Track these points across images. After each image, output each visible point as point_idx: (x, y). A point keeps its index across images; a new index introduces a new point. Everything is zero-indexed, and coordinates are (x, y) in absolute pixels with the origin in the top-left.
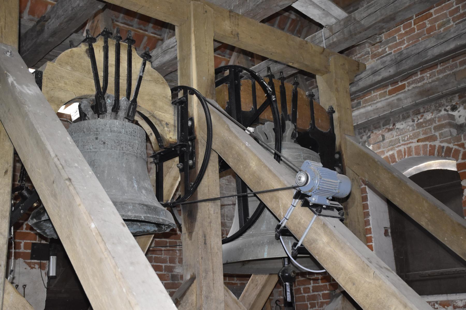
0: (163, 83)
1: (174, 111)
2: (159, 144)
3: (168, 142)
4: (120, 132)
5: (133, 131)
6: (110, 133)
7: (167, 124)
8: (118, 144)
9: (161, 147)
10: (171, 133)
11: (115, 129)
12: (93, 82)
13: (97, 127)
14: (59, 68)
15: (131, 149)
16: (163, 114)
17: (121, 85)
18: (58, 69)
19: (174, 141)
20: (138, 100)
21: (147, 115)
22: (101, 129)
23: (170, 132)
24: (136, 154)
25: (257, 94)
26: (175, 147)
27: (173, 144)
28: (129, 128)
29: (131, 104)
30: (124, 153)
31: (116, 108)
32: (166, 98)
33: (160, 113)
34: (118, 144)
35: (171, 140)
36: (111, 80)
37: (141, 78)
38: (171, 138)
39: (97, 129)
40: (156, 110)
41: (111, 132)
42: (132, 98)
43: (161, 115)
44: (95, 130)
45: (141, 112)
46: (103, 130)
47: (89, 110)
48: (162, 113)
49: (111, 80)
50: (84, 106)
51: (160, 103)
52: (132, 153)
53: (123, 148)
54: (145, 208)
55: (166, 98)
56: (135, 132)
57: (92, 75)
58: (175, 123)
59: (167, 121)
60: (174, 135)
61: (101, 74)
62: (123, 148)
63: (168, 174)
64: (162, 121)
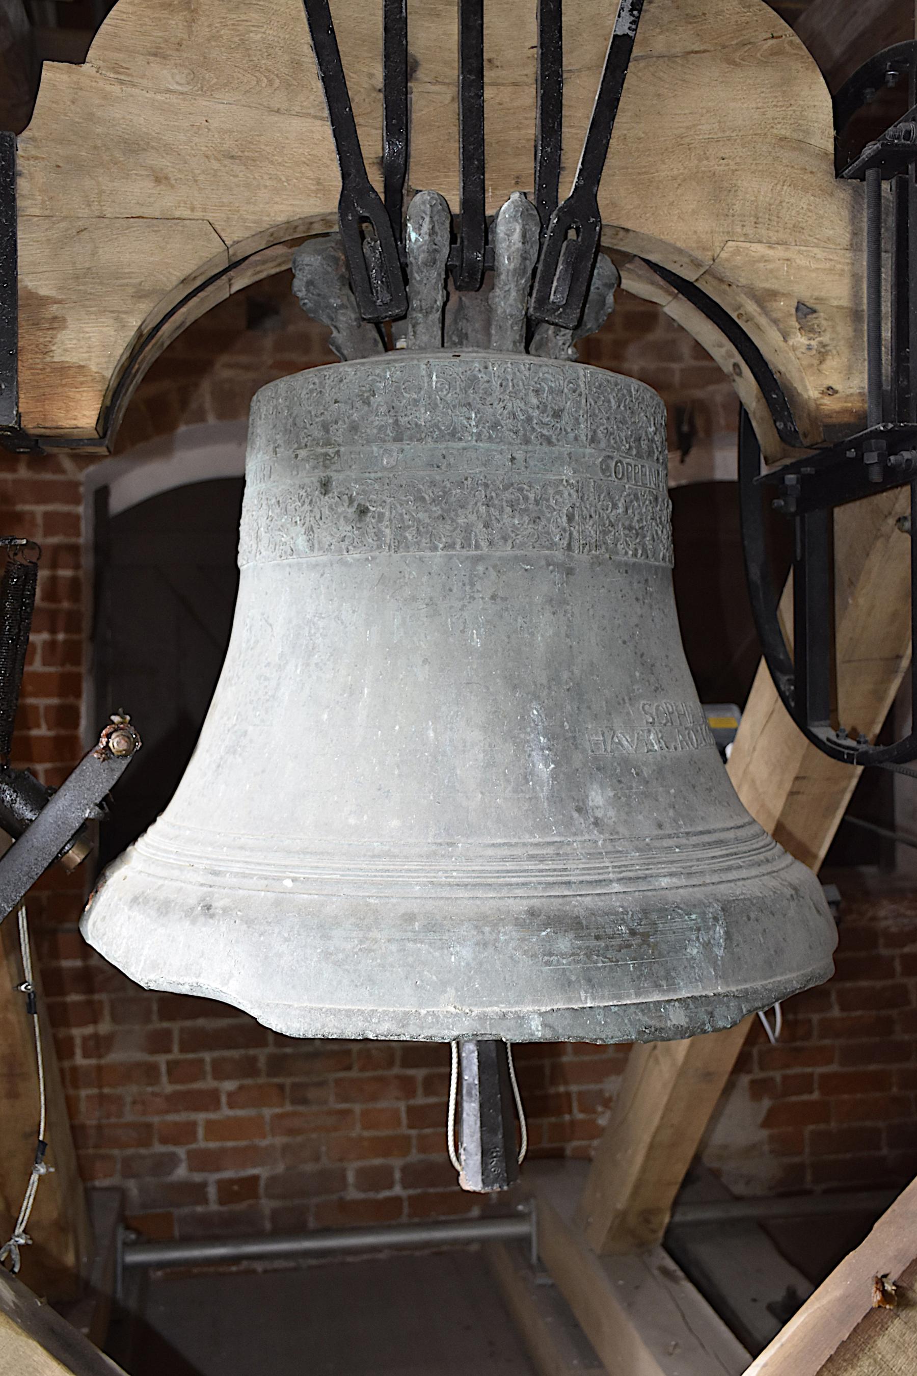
0: (777, 52)
1: (854, 219)
2: (780, 425)
3: (816, 418)
4: (454, 434)
5: (543, 408)
6: (395, 446)
7: (804, 311)
8: (437, 510)
9: (788, 437)
10: (832, 363)
11: (424, 417)
12: (323, 133)
13: (328, 417)
14: (116, 89)
15: (530, 528)
16: (779, 252)
17: (493, 125)
18: (106, 96)
19: (856, 405)
20: (604, 195)
21: (689, 275)
22: (342, 426)
23: (823, 354)
24: (559, 555)
25: (326, 130)
26: (858, 444)
27: (848, 426)
28: (515, 394)
29: (561, 232)
30: (478, 559)
31: (468, 265)
32: (800, 145)
33: (759, 249)
34: (437, 510)
35: (830, 404)
36: (434, 101)
37: (621, 51)
38: (830, 391)
39: (326, 427)
40: (731, 236)
41: (398, 439)
42: (567, 190)
43: (764, 259)
44: (318, 433)
45: (653, 258)
46: (354, 428)
47: (335, 302)
48: (771, 245)
49: (434, 101)
50: (310, 283)
51: (754, 188)
52: (530, 552)
53: (468, 529)
54: (564, 943)
55: (800, 145)
56: (557, 415)
57: (315, 91)
58: (856, 295)
59: (802, 291)
60: (849, 371)
61: (365, 74)
62: (468, 529)
63: (879, 544)
64: (773, 294)
